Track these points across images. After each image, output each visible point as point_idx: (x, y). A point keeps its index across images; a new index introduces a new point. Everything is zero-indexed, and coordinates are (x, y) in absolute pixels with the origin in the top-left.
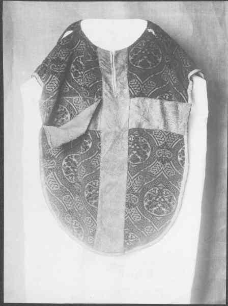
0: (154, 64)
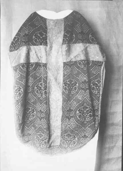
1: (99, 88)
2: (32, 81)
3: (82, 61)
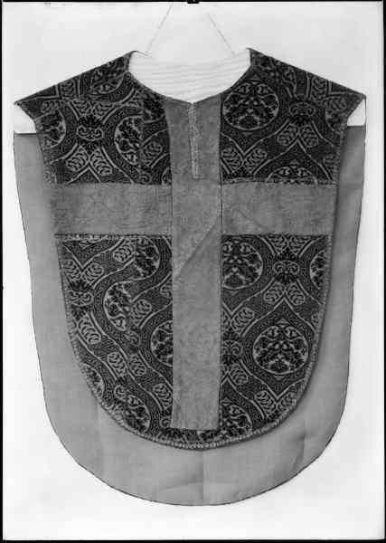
0: (249, 279)
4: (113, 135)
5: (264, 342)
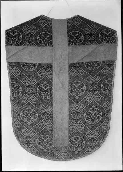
0: (103, 33)
1: (110, 88)
2: (35, 81)
3: (91, 63)
4: (101, 86)
5: (82, 91)
